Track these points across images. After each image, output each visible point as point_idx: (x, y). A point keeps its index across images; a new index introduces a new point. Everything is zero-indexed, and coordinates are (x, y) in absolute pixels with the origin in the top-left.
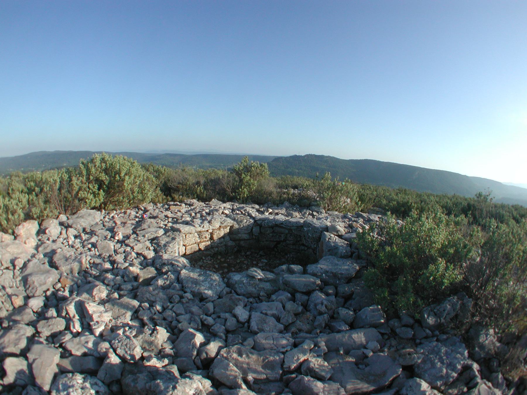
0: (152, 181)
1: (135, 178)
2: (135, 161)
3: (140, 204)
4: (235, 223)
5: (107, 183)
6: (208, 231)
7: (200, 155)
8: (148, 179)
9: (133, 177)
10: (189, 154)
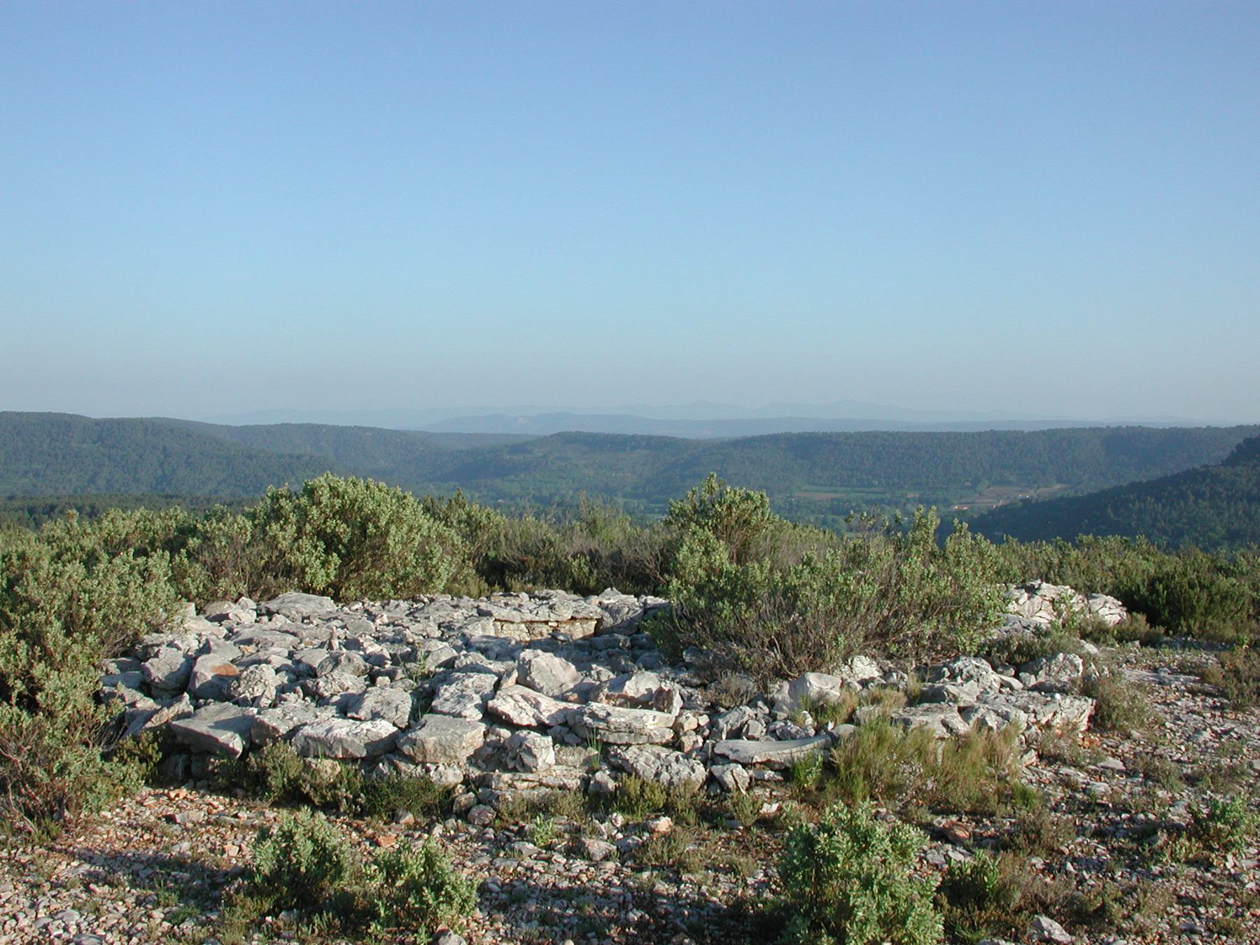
0: (453, 545)
1: (411, 529)
2: (409, 494)
3: (419, 590)
4: (607, 614)
5: (345, 541)
6: (546, 622)
7: (775, 439)
8: (441, 539)
9: (405, 528)
10: (706, 434)
